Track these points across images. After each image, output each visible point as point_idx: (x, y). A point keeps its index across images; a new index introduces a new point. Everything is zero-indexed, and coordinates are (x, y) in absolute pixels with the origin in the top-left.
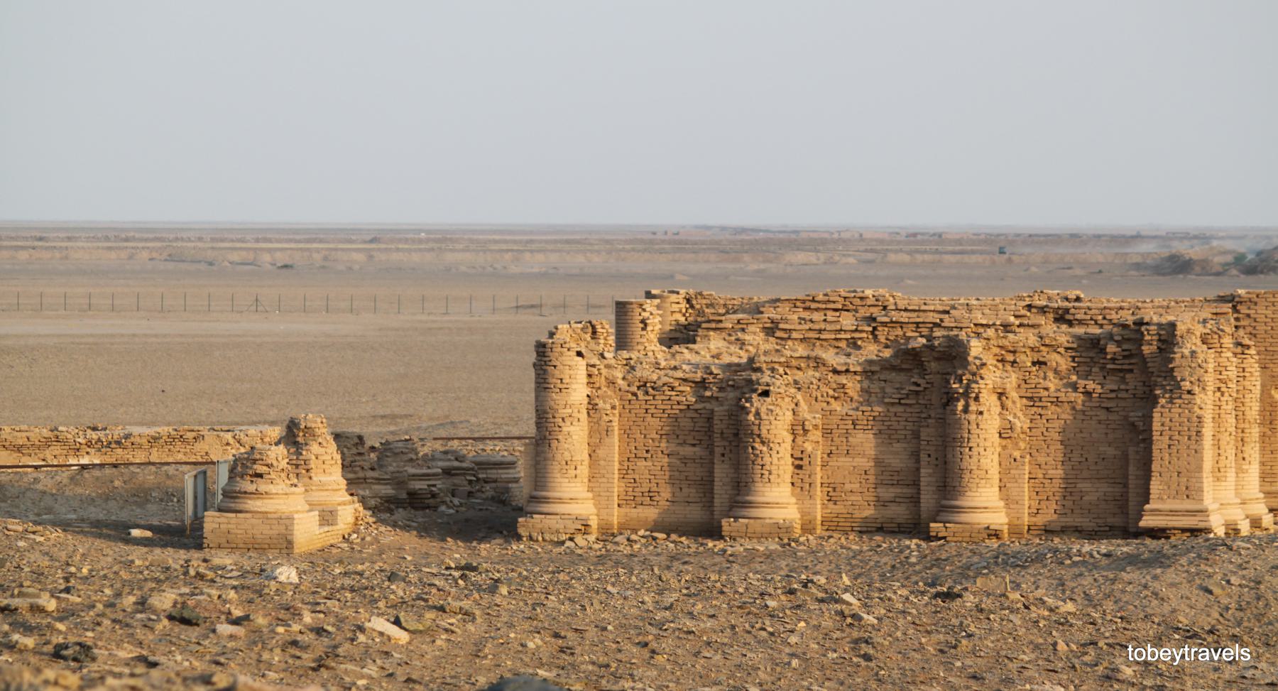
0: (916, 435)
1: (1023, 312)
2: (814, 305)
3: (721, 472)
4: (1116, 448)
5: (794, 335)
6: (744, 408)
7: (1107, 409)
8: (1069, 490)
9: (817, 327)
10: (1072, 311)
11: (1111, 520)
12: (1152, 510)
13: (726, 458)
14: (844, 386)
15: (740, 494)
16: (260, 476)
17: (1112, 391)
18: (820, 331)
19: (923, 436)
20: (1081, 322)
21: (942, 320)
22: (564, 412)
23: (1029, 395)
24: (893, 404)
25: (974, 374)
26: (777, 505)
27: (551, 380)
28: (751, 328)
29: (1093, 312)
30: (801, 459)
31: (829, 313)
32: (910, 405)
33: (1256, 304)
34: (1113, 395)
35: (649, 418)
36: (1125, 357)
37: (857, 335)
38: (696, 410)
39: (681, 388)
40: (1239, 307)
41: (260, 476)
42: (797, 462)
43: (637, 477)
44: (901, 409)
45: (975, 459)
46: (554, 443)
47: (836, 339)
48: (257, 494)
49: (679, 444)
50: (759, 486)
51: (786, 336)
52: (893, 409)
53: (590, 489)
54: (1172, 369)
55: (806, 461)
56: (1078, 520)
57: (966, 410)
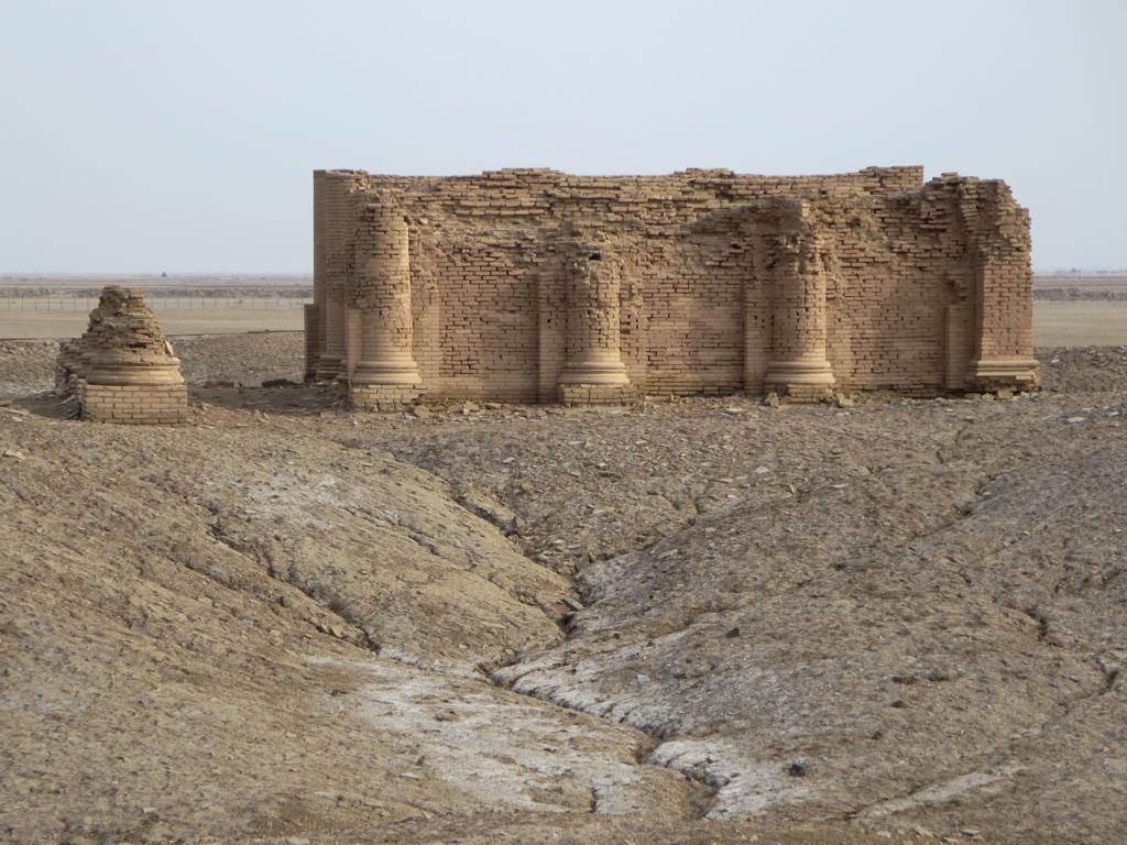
0: (741, 298)
1: (688, 188)
2: (489, 183)
3: (549, 338)
4: (931, 307)
5: (476, 212)
6: (575, 272)
7: (920, 268)
8: (883, 348)
9: (498, 203)
10: (733, 187)
11: (927, 378)
12: (985, 366)
13: (552, 324)
14: (661, 250)
15: (574, 355)
16: (143, 346)
17: (926, 251)
18: (499, 208)
19: (750, 295)
20: (742, 197)
21: (618, 196)
22: (395, 279)
23: (845, 256)
24: (713, 267)
25: (808, 235)
26: (811, 370)
27: (381, 246)
28: (433, 205)
29: (754, 187)
30: (628, 323)
31: (505, 191)
32: (730, 268)
33: (900, 178)
34: (927, 255)
35: (468, 286)
36: (938, 217)
37: (535, 211)
38: (515, 277)
39: (496, 255)
40: (884, 182)
41: (143, 346)
42: (624, 327)
43: (455, 345)
44: (722, 272)
45: (811, 319)
46: (386, 312)
47: (515, 216)
48: (143, 366)
49: (498, 311)
50: (597, 352)
51: (467, 212)
52: (715, 272)
53: (415, 358)
54: (998, 227)
55: (633, 324)
56: (893, 379)
57: (802, 270)
